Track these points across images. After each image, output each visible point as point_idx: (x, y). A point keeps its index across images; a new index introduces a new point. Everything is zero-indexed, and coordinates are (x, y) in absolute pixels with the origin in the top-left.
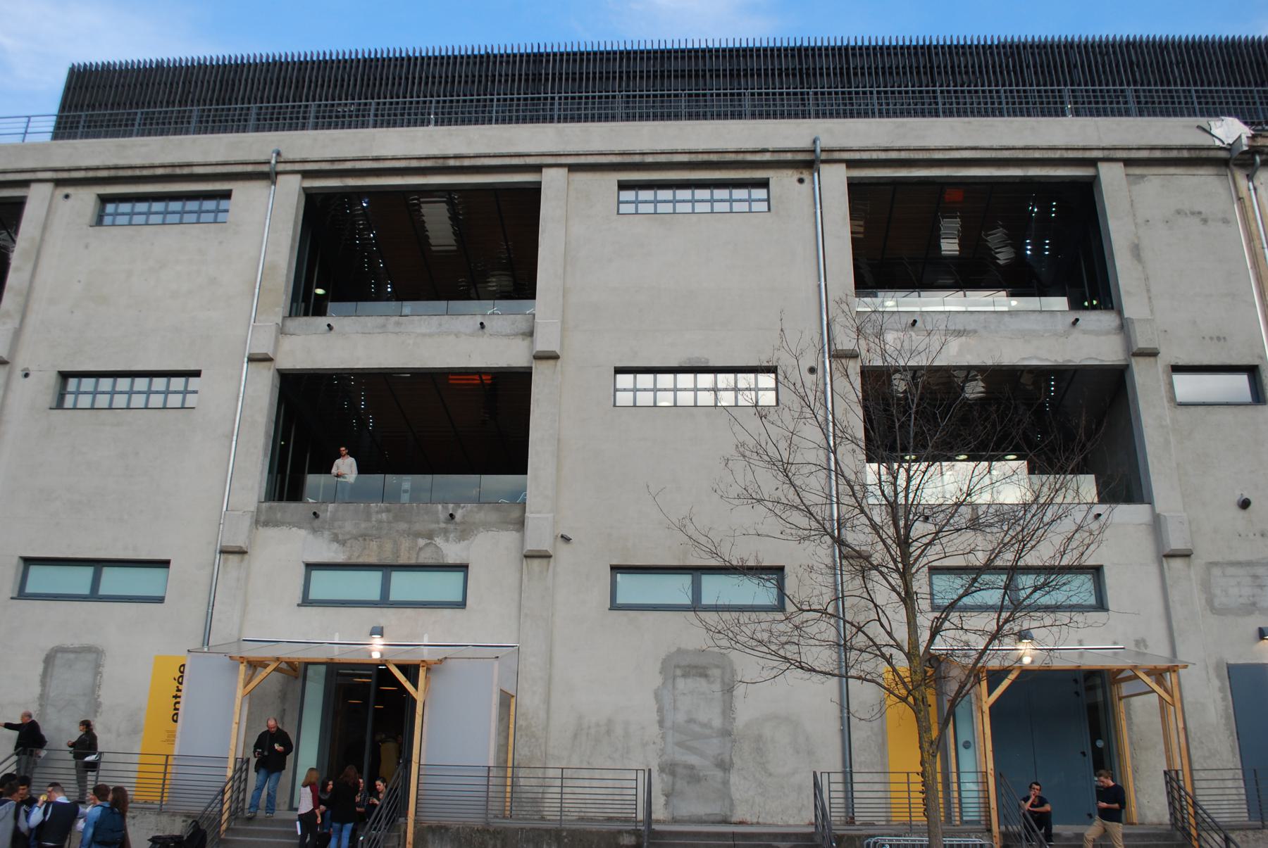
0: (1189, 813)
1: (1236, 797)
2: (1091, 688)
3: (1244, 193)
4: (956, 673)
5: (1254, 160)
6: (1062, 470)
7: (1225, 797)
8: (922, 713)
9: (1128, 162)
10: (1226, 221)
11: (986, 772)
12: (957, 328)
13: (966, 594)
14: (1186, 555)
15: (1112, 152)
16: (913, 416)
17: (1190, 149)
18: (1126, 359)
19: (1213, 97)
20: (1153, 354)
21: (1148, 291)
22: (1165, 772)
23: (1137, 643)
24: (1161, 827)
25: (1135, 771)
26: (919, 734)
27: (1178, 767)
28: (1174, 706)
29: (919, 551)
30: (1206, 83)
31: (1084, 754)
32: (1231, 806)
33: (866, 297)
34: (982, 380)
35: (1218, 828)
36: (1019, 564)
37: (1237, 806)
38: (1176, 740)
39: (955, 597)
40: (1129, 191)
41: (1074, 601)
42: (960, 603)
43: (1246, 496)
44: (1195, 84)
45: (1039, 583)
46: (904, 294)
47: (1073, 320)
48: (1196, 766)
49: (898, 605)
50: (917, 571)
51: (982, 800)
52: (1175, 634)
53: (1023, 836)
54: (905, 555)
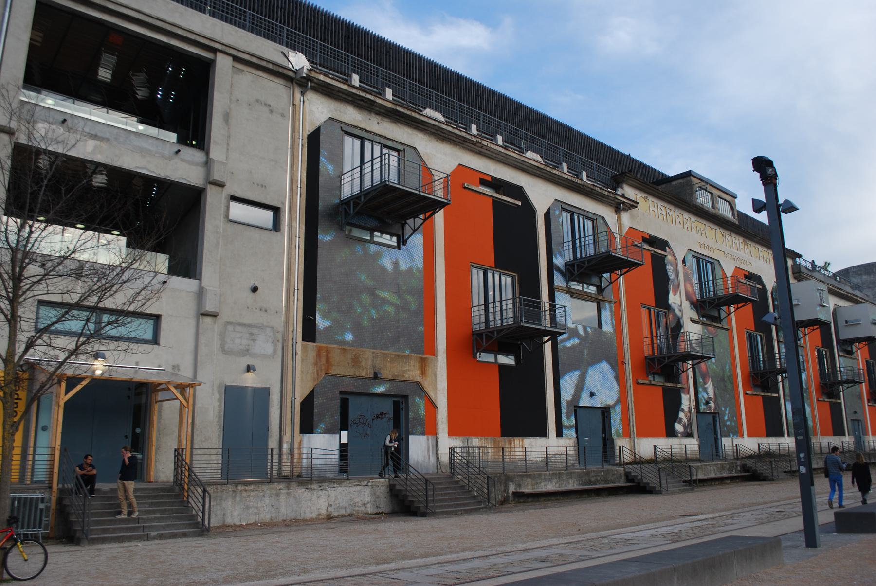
0: (185, 475)
1: (216, 466)
2: (139, 394)
3: (297, 102)
4: (42, 378)
5: (308, 84)
6: (142, 247)
7: (210, 466)
8: (9, 404)
9: (236, 59)
10: (283, 115)
11: (55, 447)
12: (96, 133)
13: (58, 322)
14: (214, 315)
15: (227, 48)
16: (44, 188)
17: (274, 64)
18: (204, 184)
19: (295, 38)
20: (221, 185)
21: (228, 145)
22: (175, 449)
23: (174, 367)
24: (168, 484)
25: (158, 449)
26: (4, 418)
27: (184, 447)
28: (188, 408)
29: (28, 286)
30: (298, 29)
31: (126, 437)
32: (212, 471)
33: (32, 91)
34: (106, 175)
35: (201, 484)
36: (99, 305)
37: (215, 471)
38: (186, 430)
39: (49, 323)
40: (232, 77)
41: (133, 335)
42: (53, 328)
43: (256, 285)
44: (288, 26)
45: (111, 320)
46: (62, 98)
47: (176, 150)
48: (196, 446)
49: (4, 323)
50: (25, 299)
51: (48, 467)
52: (198, 364)
53: (74, 491)
54: (16, 288)
